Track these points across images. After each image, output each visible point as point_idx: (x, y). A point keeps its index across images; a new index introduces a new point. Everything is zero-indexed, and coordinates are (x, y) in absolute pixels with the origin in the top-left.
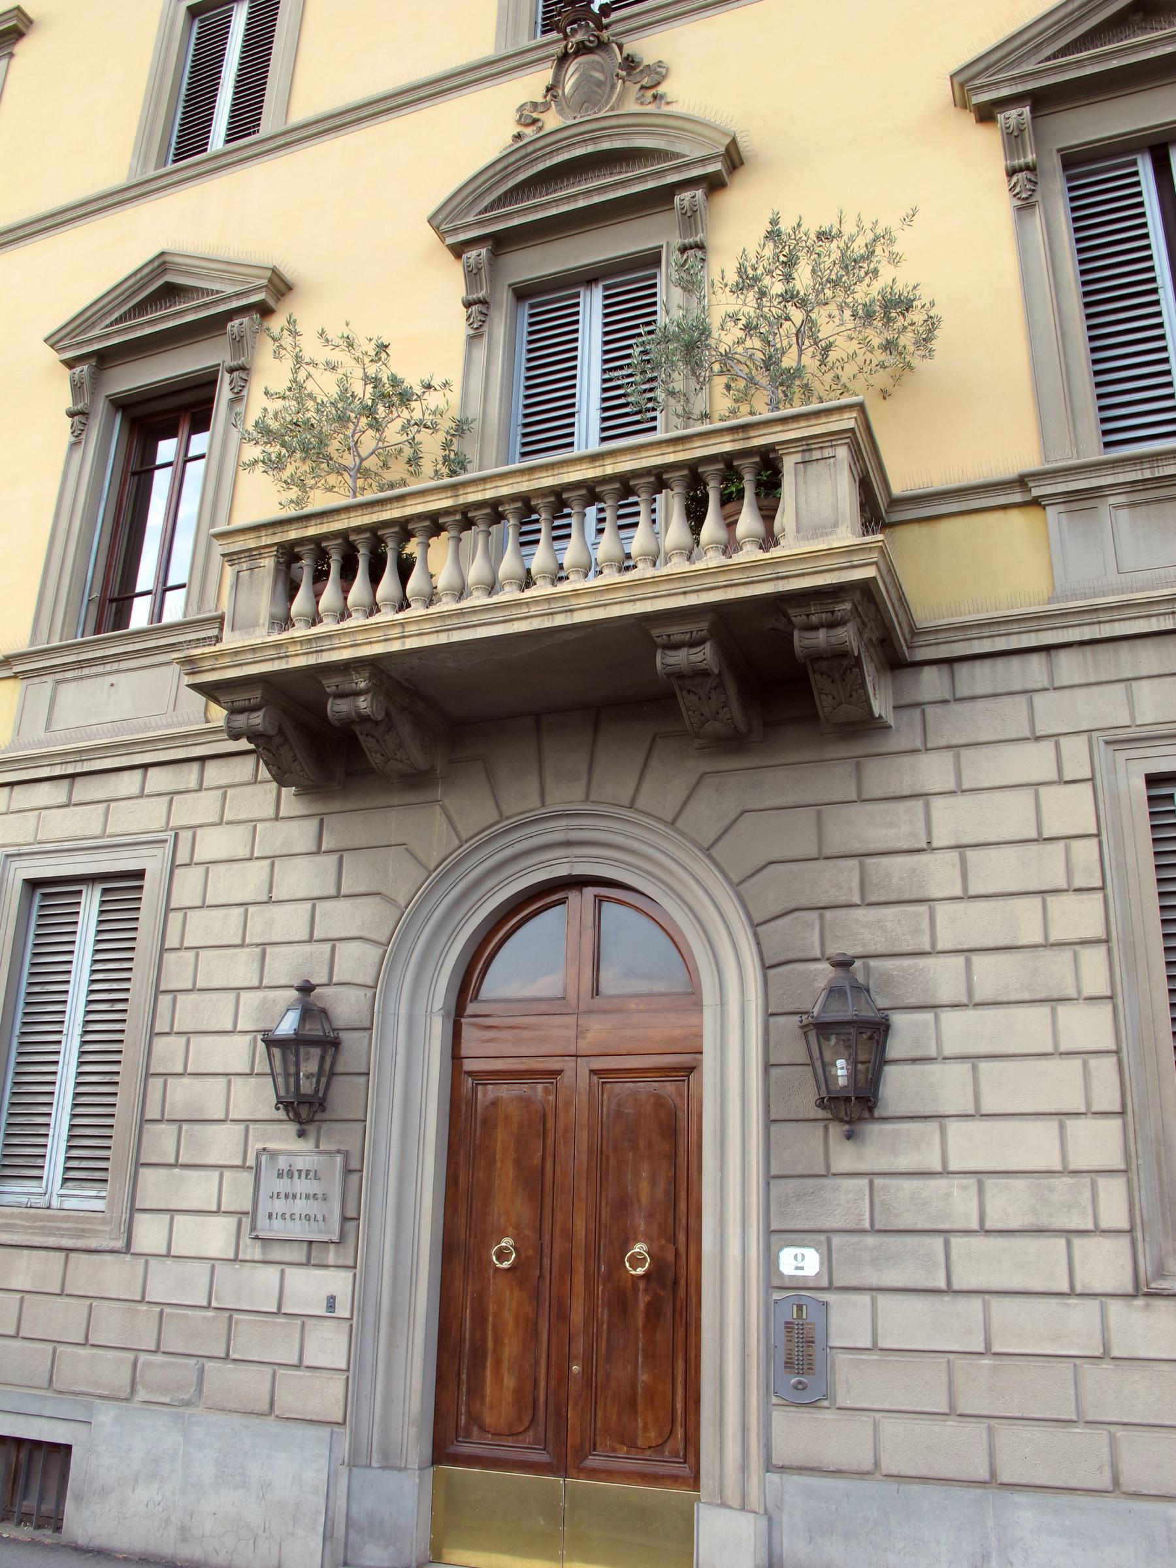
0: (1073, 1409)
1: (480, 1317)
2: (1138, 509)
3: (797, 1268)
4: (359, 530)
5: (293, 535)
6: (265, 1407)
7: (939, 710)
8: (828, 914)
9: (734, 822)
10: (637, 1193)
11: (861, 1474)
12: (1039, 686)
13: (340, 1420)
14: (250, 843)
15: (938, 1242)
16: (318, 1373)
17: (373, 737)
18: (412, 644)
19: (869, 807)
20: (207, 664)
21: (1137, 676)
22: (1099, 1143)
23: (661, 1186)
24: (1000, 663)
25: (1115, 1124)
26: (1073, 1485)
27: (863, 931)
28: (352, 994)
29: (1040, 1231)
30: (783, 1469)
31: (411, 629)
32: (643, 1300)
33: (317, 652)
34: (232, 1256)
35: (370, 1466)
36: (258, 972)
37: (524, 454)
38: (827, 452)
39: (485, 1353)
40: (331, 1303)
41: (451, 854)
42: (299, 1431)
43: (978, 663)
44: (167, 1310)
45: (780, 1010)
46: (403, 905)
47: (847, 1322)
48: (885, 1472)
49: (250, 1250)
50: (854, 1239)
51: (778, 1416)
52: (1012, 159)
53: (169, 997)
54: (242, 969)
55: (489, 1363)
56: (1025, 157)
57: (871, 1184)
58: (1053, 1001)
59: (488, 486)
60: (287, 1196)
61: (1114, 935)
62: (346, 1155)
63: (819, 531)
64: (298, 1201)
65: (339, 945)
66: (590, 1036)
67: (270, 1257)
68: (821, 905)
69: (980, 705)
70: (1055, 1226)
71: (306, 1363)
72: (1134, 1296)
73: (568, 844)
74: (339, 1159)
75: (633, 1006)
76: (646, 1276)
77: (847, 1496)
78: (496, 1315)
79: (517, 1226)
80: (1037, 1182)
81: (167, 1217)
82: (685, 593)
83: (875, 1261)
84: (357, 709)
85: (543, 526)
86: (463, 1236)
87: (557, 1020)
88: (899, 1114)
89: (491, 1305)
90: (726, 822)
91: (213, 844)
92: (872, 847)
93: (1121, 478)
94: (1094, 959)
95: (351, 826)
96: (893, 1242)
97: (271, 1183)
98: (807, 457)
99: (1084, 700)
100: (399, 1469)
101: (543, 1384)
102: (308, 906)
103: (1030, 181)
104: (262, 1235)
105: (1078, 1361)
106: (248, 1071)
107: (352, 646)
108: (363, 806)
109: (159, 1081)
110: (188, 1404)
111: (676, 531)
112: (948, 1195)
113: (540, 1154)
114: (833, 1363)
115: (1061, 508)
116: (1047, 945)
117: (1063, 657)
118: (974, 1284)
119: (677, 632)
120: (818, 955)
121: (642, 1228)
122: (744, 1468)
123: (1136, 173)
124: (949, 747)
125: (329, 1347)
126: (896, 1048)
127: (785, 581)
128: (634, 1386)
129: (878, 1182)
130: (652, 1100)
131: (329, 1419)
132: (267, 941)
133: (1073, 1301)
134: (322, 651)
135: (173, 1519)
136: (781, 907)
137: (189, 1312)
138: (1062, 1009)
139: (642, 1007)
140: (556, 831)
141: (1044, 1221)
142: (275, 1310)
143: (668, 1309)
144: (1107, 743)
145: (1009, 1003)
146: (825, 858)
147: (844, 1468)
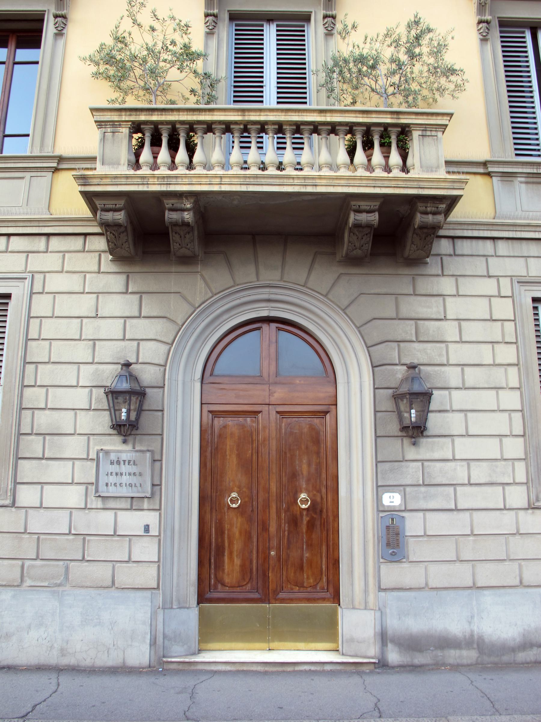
0: (505, 555)
1: (220, 531)
2: (529, 185)
3: (391, 502)
4: (183, 123)
5: (143, 117)
6: (110, 584)
7: (449, 258)
8: (402, 344)
9: (356, 298)
10: (301, 470)
11: (420, 589)
12: (490, 254)
13: (156, 587)
14: (82, 284)
15: (451, 489)
16: (140, 564)
17: (179, 234)
18: (225, 188)
19: (419, 298)
20: (95, 181)
21: (529, 255)
22: (515, 448)
23: (313, 467)
24: (474, 242)
25: (521, 440)
26: (505, 584)
27: (418, 353)
28: (152, 369)
29: (492, 484)
30: (385, 590)
31: (225, 180)
32: (305, 519)
33: (167, 184)
34: (83, 506)
35: (172, 608)
36: (91, 354)
37: (234, 101)
38: (434, 133)
39: (224, 549)
40: (147, 528)
41: (207, 300)
42: (132, 594)
43: (465, 240)
44: (42, 537)
45: (380, 387)
46: (181, 324)
47: (413, 525)
48: (430, 587)
49: (94, 503)
50: (416, 488)
51: (383, 567)
52: (208, 10)
53: (33, 366)
54: (81, 352)
55: (226, 553)
56: (214, 10)
57: (423, 464)
58: (497, 388)
59: (262, 114)
60: (117, 474)
61: (521, 363)
62: (152, 452)
63: (430, 169)
64: (124, 476)
65: (142, 343)
66: (276, 395)
67: (108, 506)
68: (399, 340)
69: (466, 259)
70: (499, 481)
71: (133, 559)
72: (527, 509)
73: (269, 301)
74: (148, 455)
75: (298, 382)
76: (307, 509)
77: (415, 598)
78: (229, 530)
79: (239, 487)
80: (491, 463)
81: (39, 487)
82: (374, 187)
83: (425, 498)
84: (183, 218)
85: (288, 141)
86: (210, 493)
87: (259, 387)
88: (434, 434)
89: (226, 526)
90: (353, 298)
91: (56, 283)
92: (421, 316)
93: (525, 170)
94: (513, 372)
95: (145, 280)
96: (432, 490)
97: (106, 467)
98: (424, 133)
99: (509, 263)
100: (188, 608)
101: (255, 562)
102: (122, 321)
103: (214, 22)
104: (102, 495)
105: (507, 536)
106: (88, 408)
107: (189, 184)
108: (153, 270)
109: (29, 413)
110: (59, 585)
111: (342, 156)
112: (455, 469)
113: (250, 452)
114: (407, 543)
115: (499, 178)
116: (495, 365)
117: (500, 243)
118: (466, 507)
119: (364, 205)
120: (398, 363)
121: (304, 486)
122: (366, 591)
123: (262, 30)
124: (453, 276)
125: (146, 550)
126: (433, 406)
127: (422, 190)
128: (302, 559)
129: (426, 464)
130: (308, 426)
131: (149, 587)
132: (96, 338)
133: (505, 512)
134: (170, 184)
135: (55, 645)
136: (380, 340)
137: (57, 537)
138: (501, 392)
139: (302, 382)
140: (264, 294)
141: (494, 480)
142: (112, 533)
143: (318, 523)
144: (518, 282)
145: (479, 388)
146: (399, 319)
147: (412, 587)
